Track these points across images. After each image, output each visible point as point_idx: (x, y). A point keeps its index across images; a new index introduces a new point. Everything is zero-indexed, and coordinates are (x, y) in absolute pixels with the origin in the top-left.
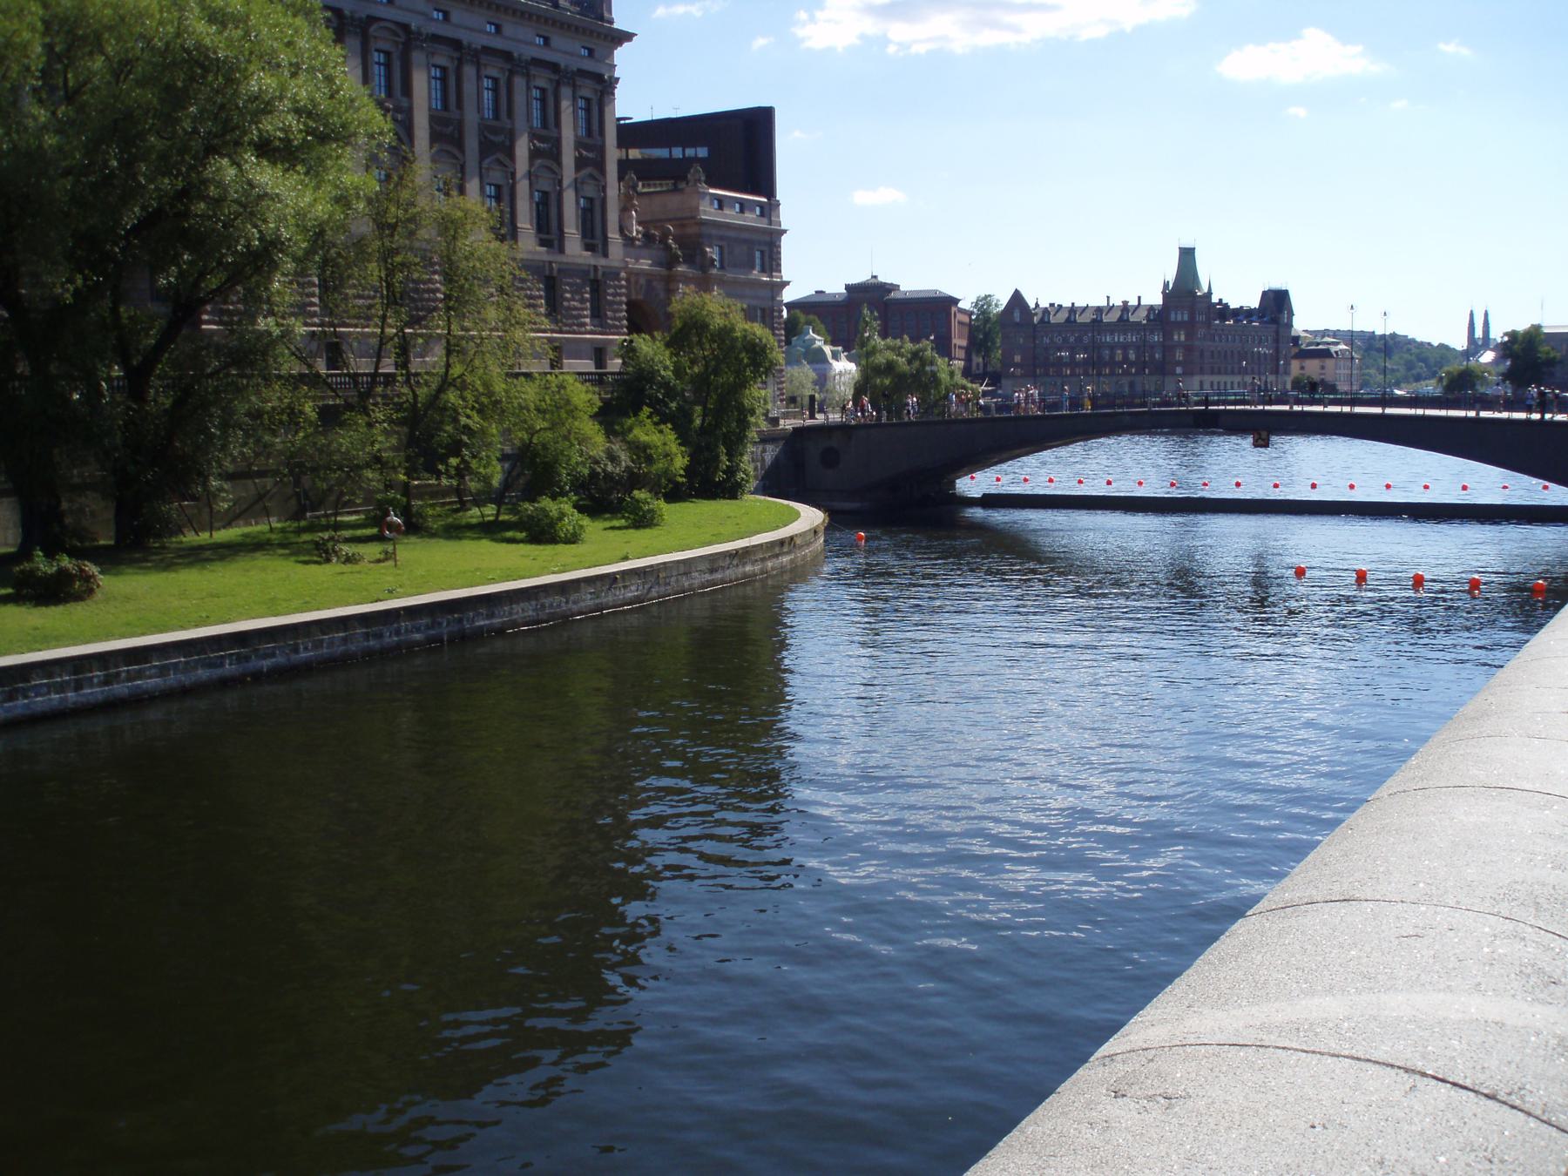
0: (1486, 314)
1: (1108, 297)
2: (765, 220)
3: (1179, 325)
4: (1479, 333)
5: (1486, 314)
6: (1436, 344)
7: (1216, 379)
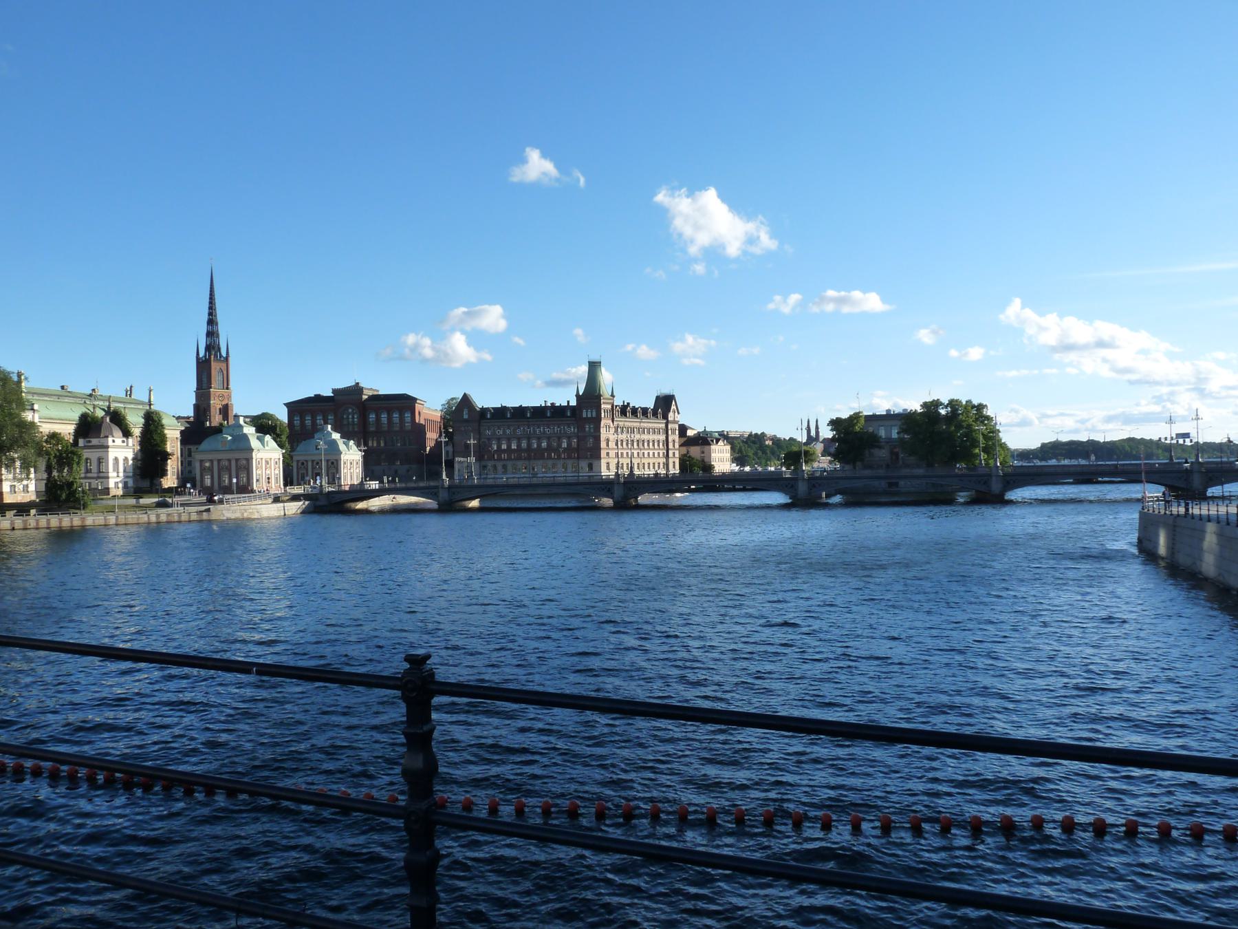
4: (813, 433)
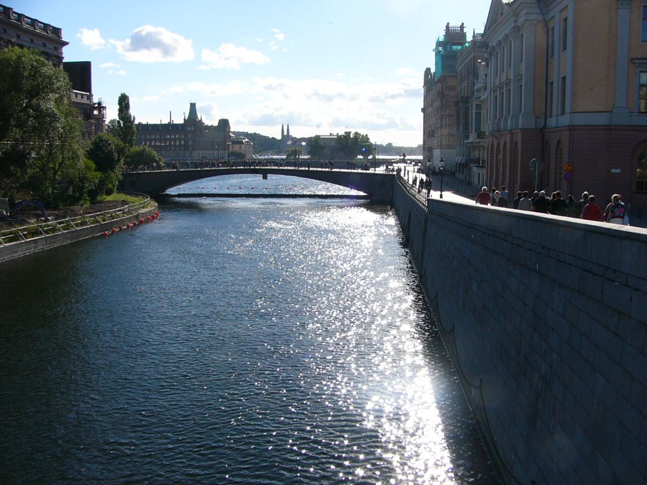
2: (89, 101)
3: (190, 132)
4: (285, 133)
6: (271, 137)
7: (204, 152)
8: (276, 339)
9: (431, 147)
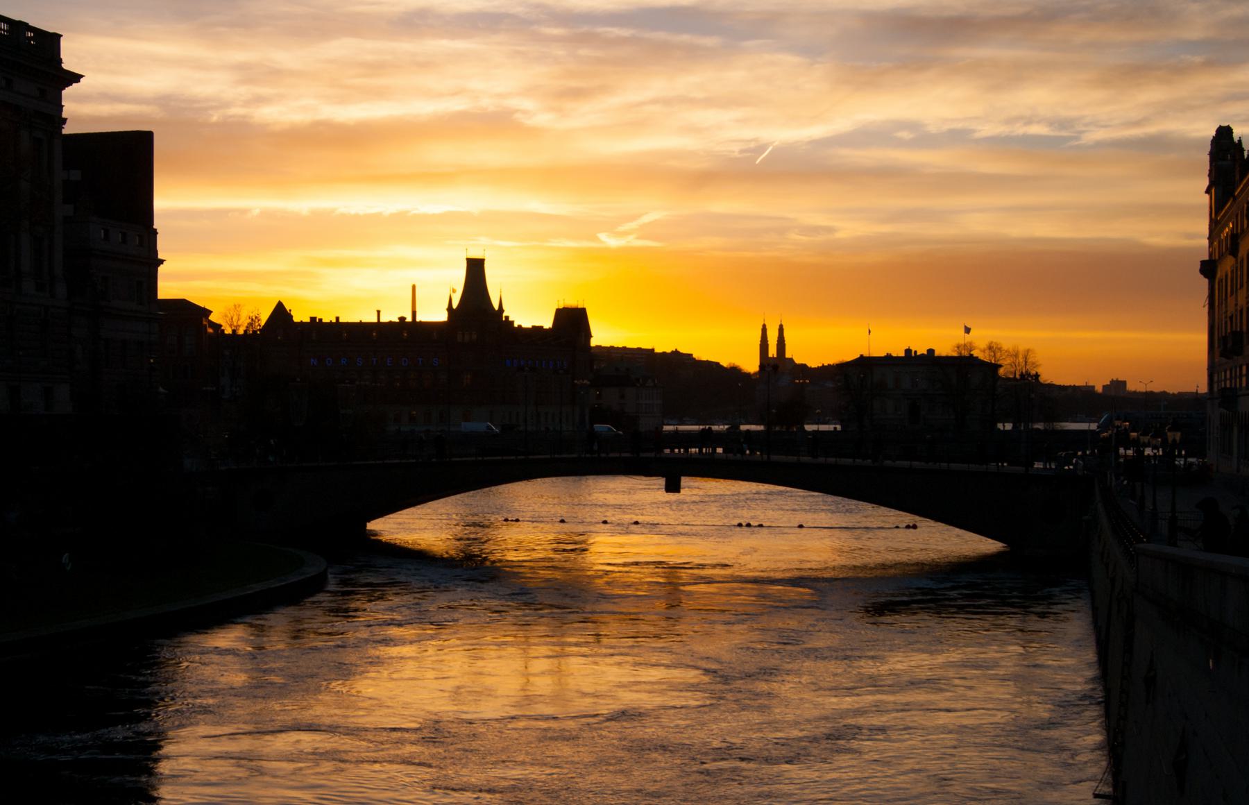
0: (781, 330)
1: (379, 312)
4: (773, 352)
5: (781, 330)
8: (1068, 715)
9: (1230, 388)
